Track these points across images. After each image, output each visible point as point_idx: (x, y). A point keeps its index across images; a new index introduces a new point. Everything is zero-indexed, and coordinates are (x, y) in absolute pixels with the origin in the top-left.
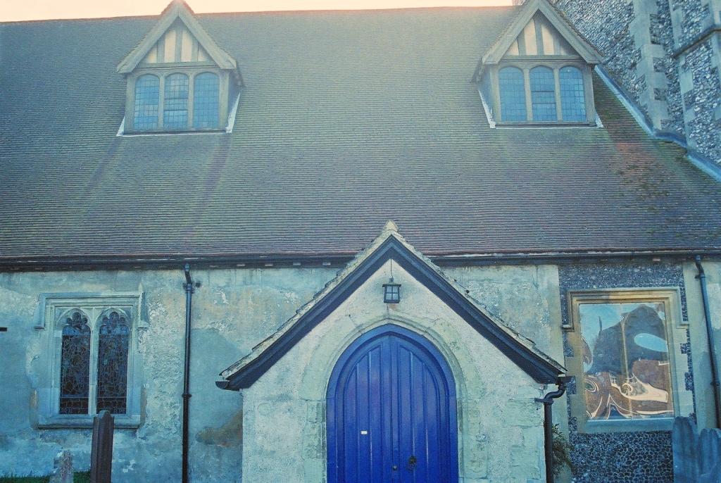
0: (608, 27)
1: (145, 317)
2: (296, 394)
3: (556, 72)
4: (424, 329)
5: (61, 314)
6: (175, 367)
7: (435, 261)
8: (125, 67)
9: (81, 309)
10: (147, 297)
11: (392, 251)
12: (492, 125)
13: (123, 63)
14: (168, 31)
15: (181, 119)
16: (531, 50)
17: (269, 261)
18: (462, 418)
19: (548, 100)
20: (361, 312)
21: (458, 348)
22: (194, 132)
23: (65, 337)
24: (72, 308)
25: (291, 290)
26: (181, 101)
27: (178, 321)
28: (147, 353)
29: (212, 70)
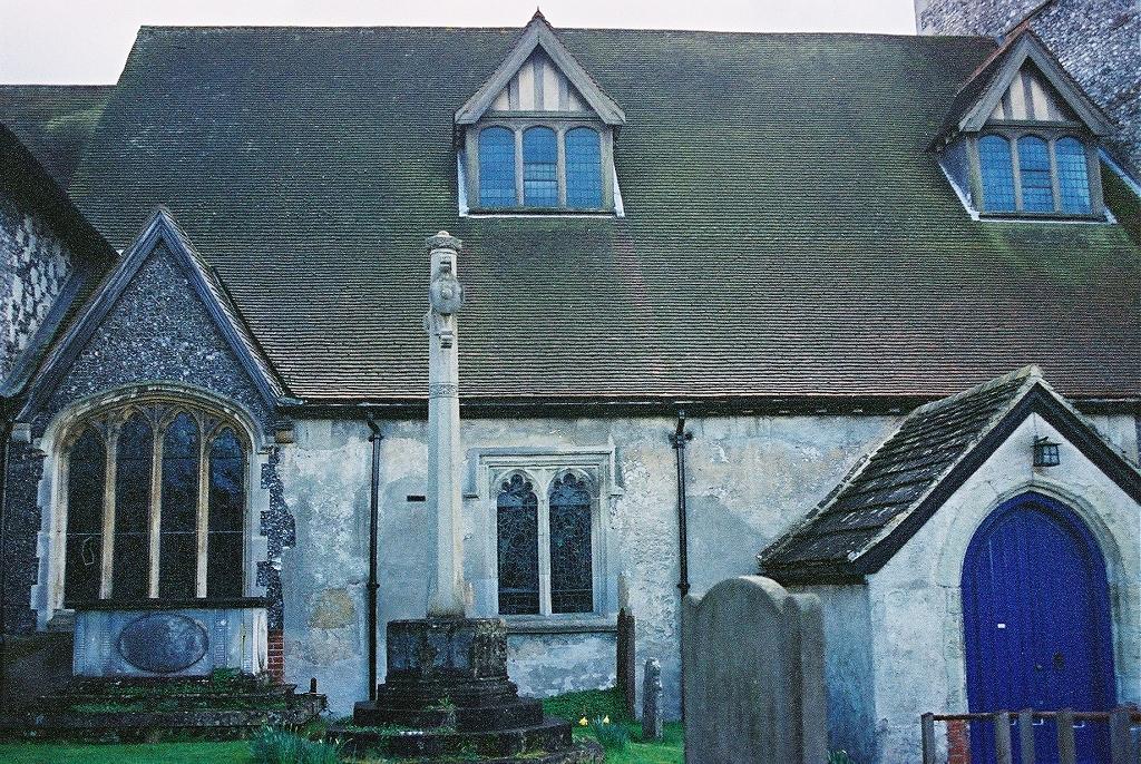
0: (1104, 80)
1: (620, 483)
2: (932, 580)
3: (1014, 144)
4: (1072, 498)
5: (496, 476)
6: (666, 548)
8: (466, 116)
9: (526, 469)
10: (621, 452)
11: (1039, 402)
12: (975, 216)
13: (464, 108)
14: (524, 65)
15: (548, 193)
16: (1019, 114)
17: (750, 406)
18: (1117, 605)
19: (1041, 183)
20: (1002, 475)
21: (1113, 521)
22: (571, 213)
23: (500, 509)
24: (513, 468)
25: (810, 444)
28: (625, 530)
29: (589, 124)
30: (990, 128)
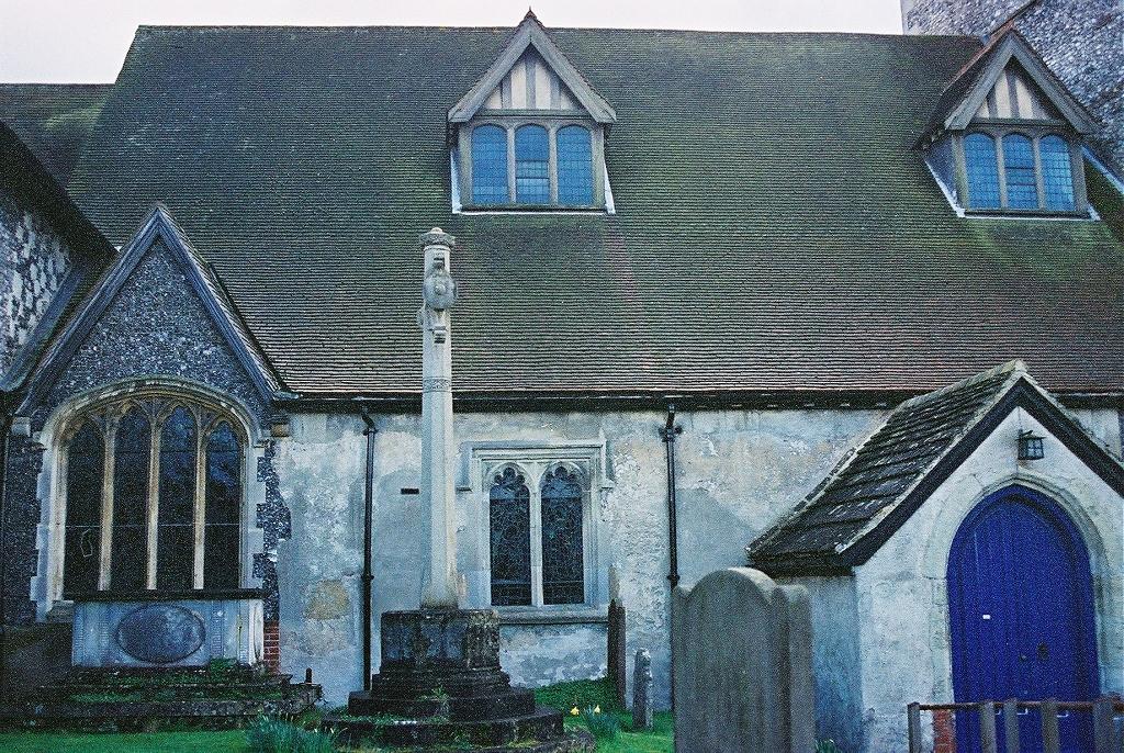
0: (1087, 79)
1: (611, 476)
2: (918, 571)
3: (999, 142)
4: (1056, 490)
5: (488, 470)
6: (656, 540)
7: (1060, 400)
8: (459, 114)
9: (518, 463)
10: (612, 446)
11: (1023, 396)
12: (960, 213)
13: (457, 107)
14: (516, 64)
15: (540, 190)
16: (1004, 112)
17: (739, 401)
18: (1101, 596)
19: (1025, 180)
20: (987, 468)
21: (1097, 514)
22: (562, 210)
23: (493, 502)
24: (506, 462)
25: (798, 438)
26: (539, 165)
27: (358, 463)
28: (616, 522)
29: (580, 122)
30: (975, 126)
